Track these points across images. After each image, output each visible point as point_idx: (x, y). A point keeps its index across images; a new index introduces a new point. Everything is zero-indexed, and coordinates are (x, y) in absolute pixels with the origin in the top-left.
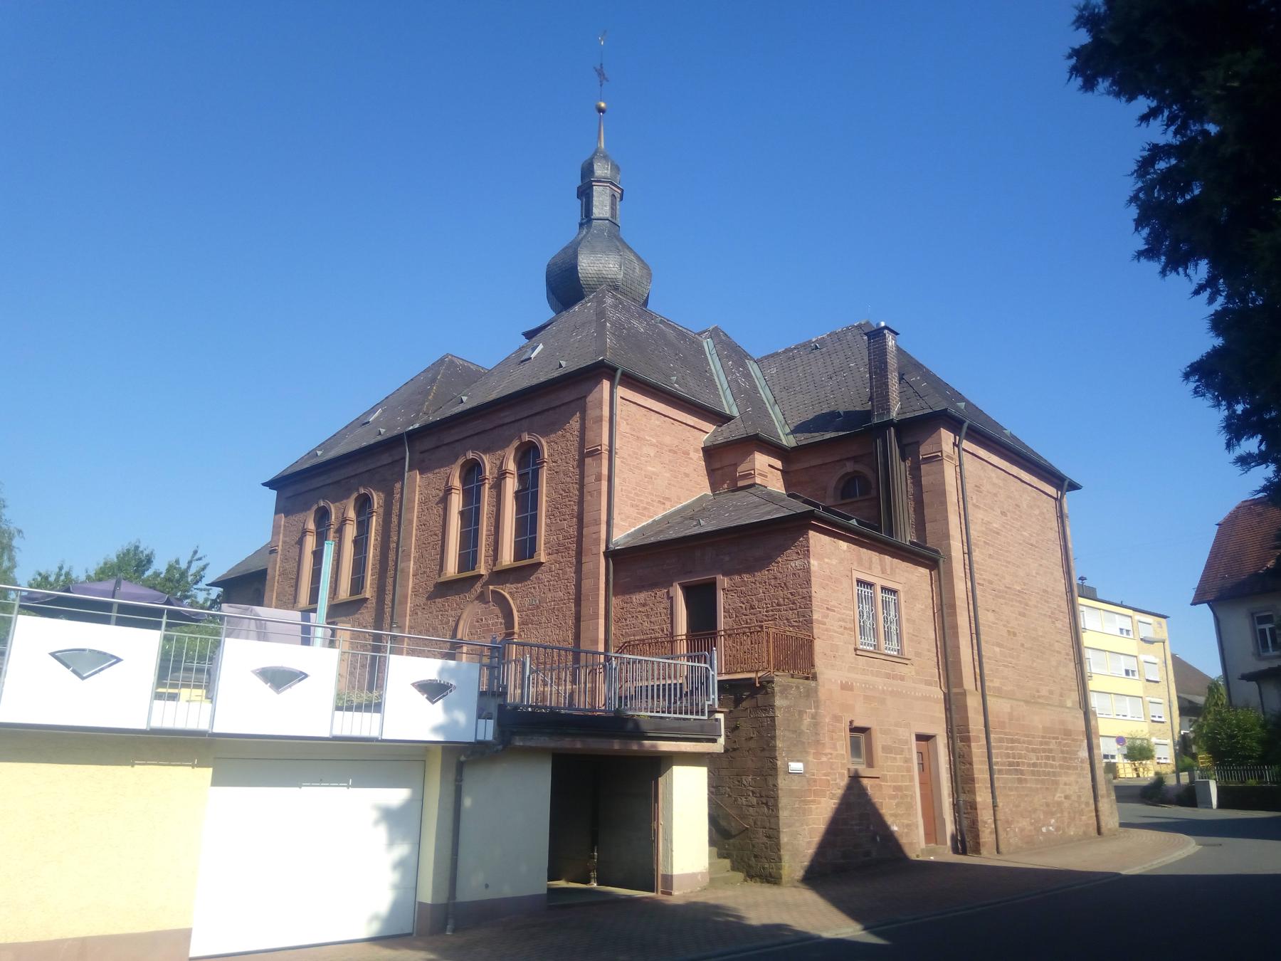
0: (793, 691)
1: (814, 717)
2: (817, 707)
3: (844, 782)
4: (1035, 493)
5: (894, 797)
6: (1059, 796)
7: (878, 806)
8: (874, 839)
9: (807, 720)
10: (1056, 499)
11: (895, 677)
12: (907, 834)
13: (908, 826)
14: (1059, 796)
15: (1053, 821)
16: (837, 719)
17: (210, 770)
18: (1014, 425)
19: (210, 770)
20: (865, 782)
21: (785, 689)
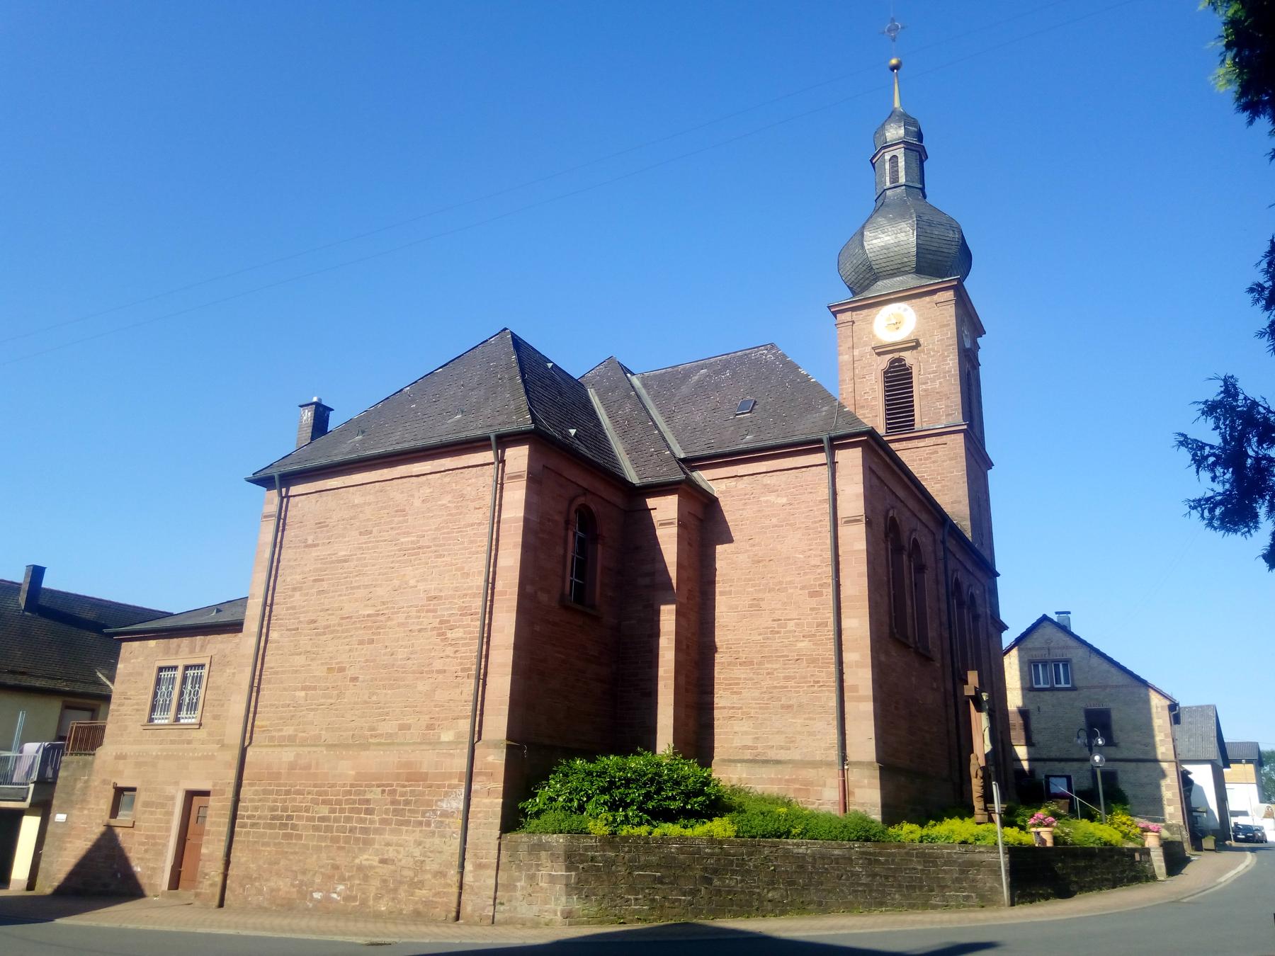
0: (74, 765)
1: (86, 782)
2: (90, 775)
3: (102, 829)
4: (447, 478)
5: (143, 844)
6: (367, 858)
7: (126, 850)
8: (115, 875)
9: (79, 785)
10: (701, 520)
11: (183, 742)
12: (150, 877)
13: (154, 869)
14: (367, 858)
15: (341, 887)
16: (104, 782)
17: (718, 547)
18: (1214, 727)
19: (718, 547)
20: (118, 830)
21: (68, 764)
